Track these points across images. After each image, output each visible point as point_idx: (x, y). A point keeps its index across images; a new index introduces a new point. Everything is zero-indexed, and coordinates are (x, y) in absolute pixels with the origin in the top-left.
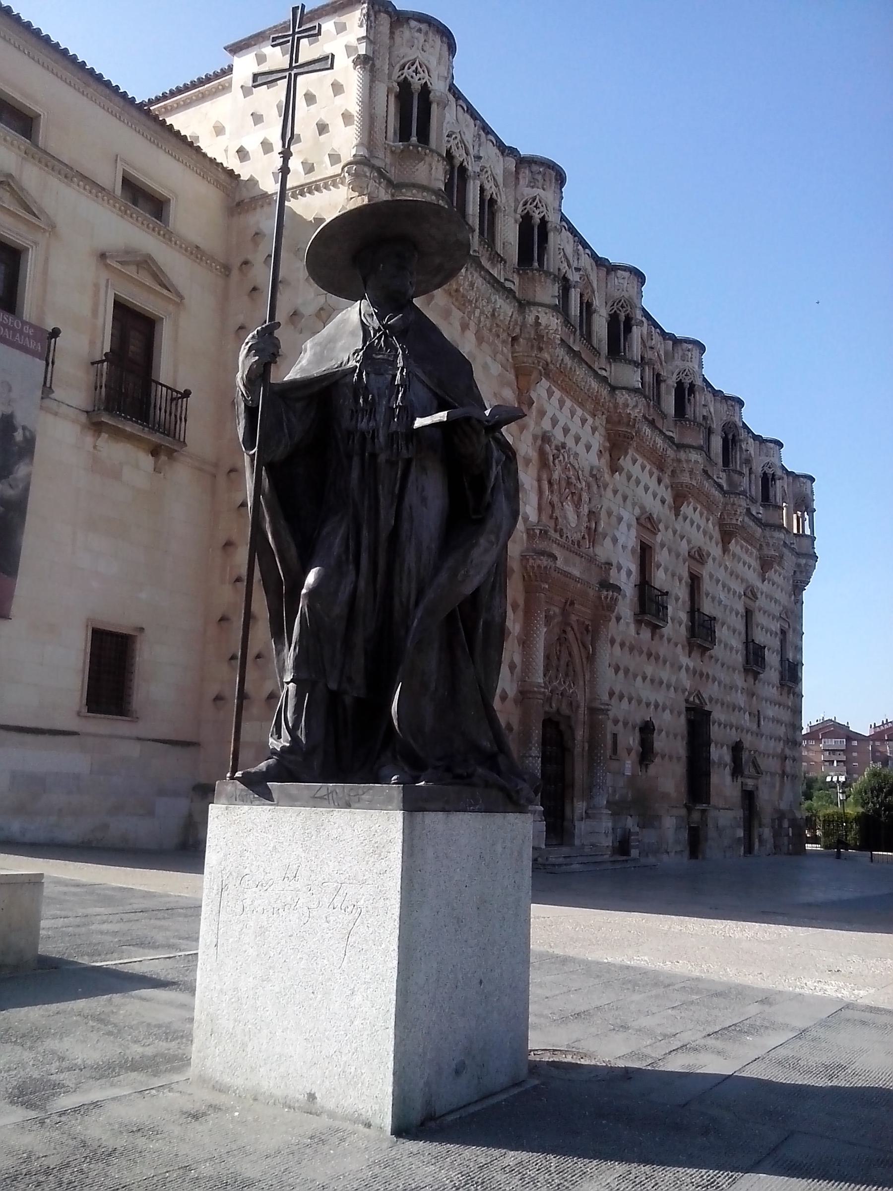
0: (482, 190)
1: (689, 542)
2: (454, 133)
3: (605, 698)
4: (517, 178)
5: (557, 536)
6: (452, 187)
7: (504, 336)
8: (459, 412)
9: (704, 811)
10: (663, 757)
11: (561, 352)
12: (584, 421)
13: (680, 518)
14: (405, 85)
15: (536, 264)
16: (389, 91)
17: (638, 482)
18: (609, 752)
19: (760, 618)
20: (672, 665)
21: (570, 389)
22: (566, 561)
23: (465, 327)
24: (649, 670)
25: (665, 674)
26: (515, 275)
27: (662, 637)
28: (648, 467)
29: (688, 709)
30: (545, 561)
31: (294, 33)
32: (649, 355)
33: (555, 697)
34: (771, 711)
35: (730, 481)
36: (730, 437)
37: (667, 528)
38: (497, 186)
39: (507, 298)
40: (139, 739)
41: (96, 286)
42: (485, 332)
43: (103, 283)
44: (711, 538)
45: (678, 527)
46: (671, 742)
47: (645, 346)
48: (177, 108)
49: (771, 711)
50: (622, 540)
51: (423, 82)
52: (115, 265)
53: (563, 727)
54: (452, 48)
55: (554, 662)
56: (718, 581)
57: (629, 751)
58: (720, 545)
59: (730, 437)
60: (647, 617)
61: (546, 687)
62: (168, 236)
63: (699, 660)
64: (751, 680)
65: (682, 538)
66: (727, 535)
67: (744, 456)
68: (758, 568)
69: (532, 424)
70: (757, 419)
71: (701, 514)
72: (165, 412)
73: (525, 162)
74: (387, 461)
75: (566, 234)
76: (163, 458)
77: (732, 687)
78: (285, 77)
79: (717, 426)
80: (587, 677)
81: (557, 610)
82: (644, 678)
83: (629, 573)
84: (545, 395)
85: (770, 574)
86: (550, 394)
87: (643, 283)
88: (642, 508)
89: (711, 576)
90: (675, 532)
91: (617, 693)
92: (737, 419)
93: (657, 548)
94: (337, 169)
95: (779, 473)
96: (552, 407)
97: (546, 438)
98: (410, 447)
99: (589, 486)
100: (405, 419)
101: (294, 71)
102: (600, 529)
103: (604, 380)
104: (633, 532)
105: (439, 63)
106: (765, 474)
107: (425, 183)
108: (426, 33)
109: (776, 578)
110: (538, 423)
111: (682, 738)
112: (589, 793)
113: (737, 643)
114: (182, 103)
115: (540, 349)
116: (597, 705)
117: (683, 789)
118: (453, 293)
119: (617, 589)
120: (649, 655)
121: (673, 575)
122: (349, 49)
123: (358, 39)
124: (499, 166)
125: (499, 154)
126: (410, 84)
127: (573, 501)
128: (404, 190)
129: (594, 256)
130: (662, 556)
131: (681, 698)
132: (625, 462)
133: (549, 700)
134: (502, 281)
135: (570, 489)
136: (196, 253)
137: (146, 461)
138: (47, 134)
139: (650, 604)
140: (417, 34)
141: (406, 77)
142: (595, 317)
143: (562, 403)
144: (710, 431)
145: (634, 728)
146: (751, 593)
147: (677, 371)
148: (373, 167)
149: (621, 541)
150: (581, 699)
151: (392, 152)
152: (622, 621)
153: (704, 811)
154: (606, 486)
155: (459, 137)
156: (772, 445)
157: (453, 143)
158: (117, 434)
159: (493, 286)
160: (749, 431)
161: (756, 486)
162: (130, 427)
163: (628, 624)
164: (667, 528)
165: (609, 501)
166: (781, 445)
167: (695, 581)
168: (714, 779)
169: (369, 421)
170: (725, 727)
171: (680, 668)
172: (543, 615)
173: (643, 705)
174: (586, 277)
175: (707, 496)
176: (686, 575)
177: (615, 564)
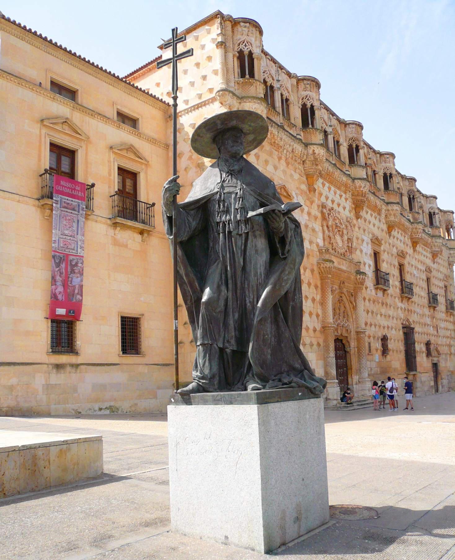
0: (282, 95)
1: (397, 248)
3: (363, 326)
4: (298, 88)
5: (333, 252)
7: (299, 161)
8: (268, 208)
9: (414, 375)
10: (393, 351)
11: (326, 165)
12: (341, 196)
13: (392, 237)
14: (241, 52)
15: (310, 126)
16: (234, 56)
17: (370, 222)
18: (367, 352)
19: (433, 281)
20: (394, 308)
21: (332, 181)
22: (339, 263)
23: (280, 158)
24: (383, 311)
25: (391, 312)
26: (301, 132)
27: (388, 295)
28: (374, 215)
29: (403, 328)
30: (328, 264)
31: (174, 41)
32: (369, 162)
33: (339, 328)
34: (442, 325)
35: (414, 218)
36: (412, 197)
37: (385, 243)
38: (288, 92)
40: (147, 364)
41: (109, 161)
42: (290, 160)
43: (112, 160)
44: (407, 245)
45: (391, 241)
46: (397, 344)
47: (366, 158)
49: (442, 325)
50: (364, 250)
51: (249, 50)
52: (116, 151)
53: (344, 342)
54: (261, 33)
55: (338, 311)
56: (412, 265)
57: (377, 350)
58: (412, 248)
59: (412, 197)
60: (380, 286)
61: (334, 324)
62: (139, 135)
63: (406, 304)
64: (432, 310)
65: (393, 246)
66: (415, 243)
67: (419, 205)
68: (431, 257)
69: (316, 200)
70: (424, 186)
71: (401, 234)
73: (300, 80)
74: (238, 234)
75: (324, 111)
76: (146, 235)
77: (423, 315)
79: (405, 192)
80: (354, 317)
81: (337, 287)
82: (381, 315)
83: (370, 266)
84: (321, 186)
85: (437, 260)
86: (324, 185)
87: (362, 129)
88: (373, 234)
89: (409, 263)
90: (390, 244)
91: (369, 323)
92: (414, 188)
93: (382, 253)
95: (437, 211)
96: (325, 191)
97: (323, 206)
98: (247, 226)
99: (346, 226)
101: (177, 58)
102: (353, 246)
103: (349, 175)
104: (370, 246)
105: (256, 40)
106: (430, 213)
107: (254, 95)
108: (248, 28)
109: (440, 261)
110: (319, 199)
111: (402, 341)
112: (359, 371)
113: (424, 294)
115: (317, 165)
116: (359, 330)
117: (404, 365)
119: (364, 274)
120: (383, 304)
121: (391, 265)
122: (213, 40)
123: (217, 35)
124: (289, 83)
125: (288, 77)
127: (339, 234)
129: (338, 119)
130: (384, 256)
131: (399, 323)
132: (363, 213)
133: (337, 330)
134: (295, 135)
135: (338, 229)
137: (138, 237)
138: (81, 97)
139: (381, 279)
140: (244, 29)
141: (241, 49)
142: (341, 147)
143: (329, 189)
144: (402, 195)
145: (378, 339)
146: (429, 270)
147: (383, 168)
149: (364, 251)
150: (352, 328)
151: (238, 83)
152: (368, 289)
153: (414, 375)
154: (354, 225)
156: (432, 199)
157: (266, 76)
158: (124, 227)
160: (420, 193)
161: (427, 218)
162: (130, 223)
163: (371, 290)
164: (385, 243)
165: (356, 233)
166: (436, 198)
167: (401, 267)
168: (418, 359)
169: (226, 216)
170: (422, 334)
171: (398, 308)
172: (330, 290)
173: (382, 327)
174: (335, 131)
175: (403, 225)
176: (397, 264)
177: (362, 262)
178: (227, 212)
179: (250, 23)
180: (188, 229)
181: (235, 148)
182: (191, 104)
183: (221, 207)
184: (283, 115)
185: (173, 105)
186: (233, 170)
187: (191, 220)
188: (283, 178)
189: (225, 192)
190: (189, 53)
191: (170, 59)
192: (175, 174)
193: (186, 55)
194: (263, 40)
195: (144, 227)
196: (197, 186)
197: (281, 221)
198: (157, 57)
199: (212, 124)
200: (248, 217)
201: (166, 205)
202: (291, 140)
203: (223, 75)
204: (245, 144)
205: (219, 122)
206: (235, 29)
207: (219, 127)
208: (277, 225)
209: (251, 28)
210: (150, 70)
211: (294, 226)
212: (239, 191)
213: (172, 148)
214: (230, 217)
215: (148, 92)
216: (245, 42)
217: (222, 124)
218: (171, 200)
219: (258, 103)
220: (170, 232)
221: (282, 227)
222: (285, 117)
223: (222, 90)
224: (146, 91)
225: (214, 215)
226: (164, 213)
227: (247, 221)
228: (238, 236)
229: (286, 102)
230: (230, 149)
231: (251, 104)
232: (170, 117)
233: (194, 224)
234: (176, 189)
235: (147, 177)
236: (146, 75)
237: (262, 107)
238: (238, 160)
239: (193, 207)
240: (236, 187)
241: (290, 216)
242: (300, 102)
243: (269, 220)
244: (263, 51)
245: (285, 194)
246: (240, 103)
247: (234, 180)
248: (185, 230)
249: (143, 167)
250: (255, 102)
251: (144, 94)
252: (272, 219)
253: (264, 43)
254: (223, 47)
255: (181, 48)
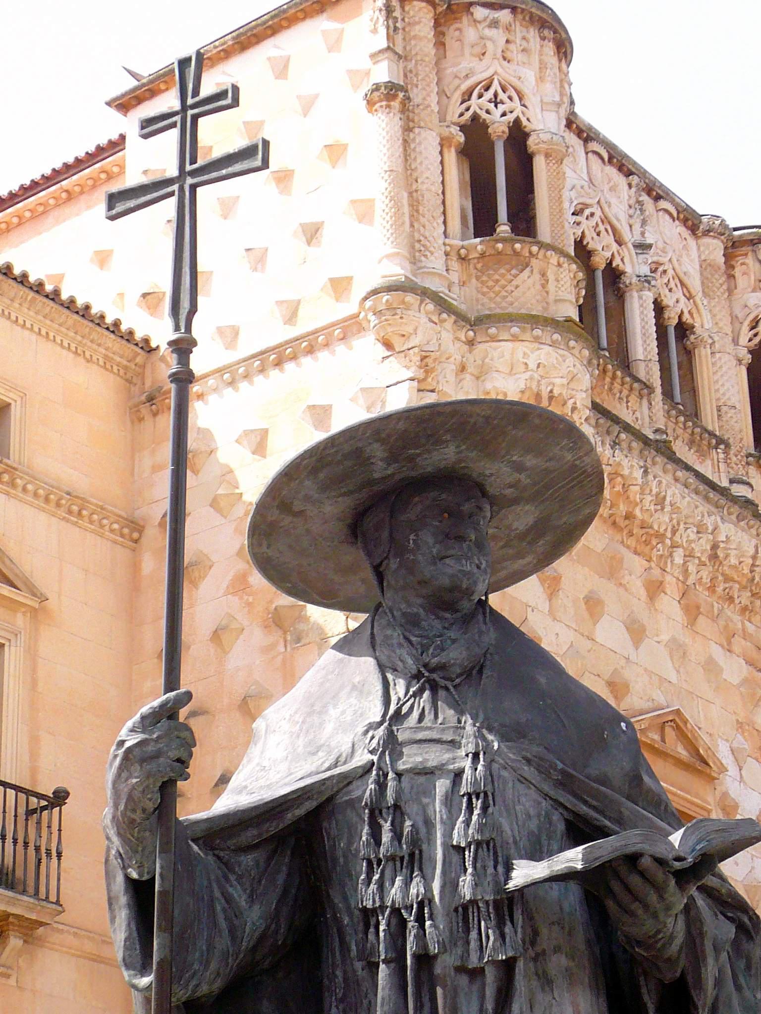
0: (659, 308)
2: (587, 206)
6: (595, 310)
8: (606, 847)
14: (475, 129)
16: (444, 142)
23: (655, 589)
39: (740, 518)
42: (702, 596)
48: (19, 224)
51: (511, 117)
54: (563, 48)
72: (15, 841)
74: (461, 969)
78: (171, 194)
94: (350, 307)
98: (508, 929)
100: (490, 870)
105: (541, 79)
108: (508, 29)
114: (28, 214)
118: (622, 523)
124: (689, 258)
125: (686, 233)
126: (485, 126)
128: (493, 331)
134: (725, 483)
136: (70, 505)
140: (488, 32)
148: (425, 293)
151: (462, 259)
155: (598, 213)
157: (587, 226)
159: (707, 498)
178: (413, 860)
179: (514, 9)
180: (223, 942)
181: (451, 567)
182: (247, 346)
183: (386, 837)
184: (668, 394)
185: (175, 378)
186: (442, 667)
187: (242, 901)
188: (673, 677)
189: (401, 766)
190: (252, 157)
191: (169, 182)
192: (172, 680)
193: (237, 167)
194: (572, 76)
195: (11, 902)
196: (273, 739)
197: (668, 908)
198: (103, 142)
199: (346, 457)
200: (511, 885)
201: (126, 826)
202: (704, 507)
203: (397, 224)
204: (494, 547)
205: (378, 451)
206: (451, 33)
207: (380, 469)
208: (649, 926)
209: (519, 31)
210: (70, 196)
211: (729, 931)
212: (467, 764)
213: (157, 541)
214: (428, 889)
215: (57, 293)
216: (496, 86)
217: (393, 458)
218: (150, 806)
219: (554, 344)
220: (141, 954)
221: (672, 937)
222: (674, 405)
223: (391, 288)
224: (49, 288)
225: (352, 877)
226: (115, 863)
227: (508, 905)
228: (464, 980)
229: (676, 338)
230: (427, 571)
231: (521, 348)
232: (151, 399)
233: (254, 917)
234: (174, 754)
235: (34, 670)
236: (50, 219)
237: (570, 360)
238: (467, 620)
239: (250, 836)
240: (455, 746)
241: (710, 881)
242: (744, 340)
243: (610, 904)
244: (572, 122)
245: (682, 752)
246: (471, 343)
247: (447, 713)
248: (210, 947)
249: (20, 620)
250: (536, 339)
251: (41, 299)
252: (625, 898)
253: (576, 91)
254: (396, 104)
255: (218, 135)
